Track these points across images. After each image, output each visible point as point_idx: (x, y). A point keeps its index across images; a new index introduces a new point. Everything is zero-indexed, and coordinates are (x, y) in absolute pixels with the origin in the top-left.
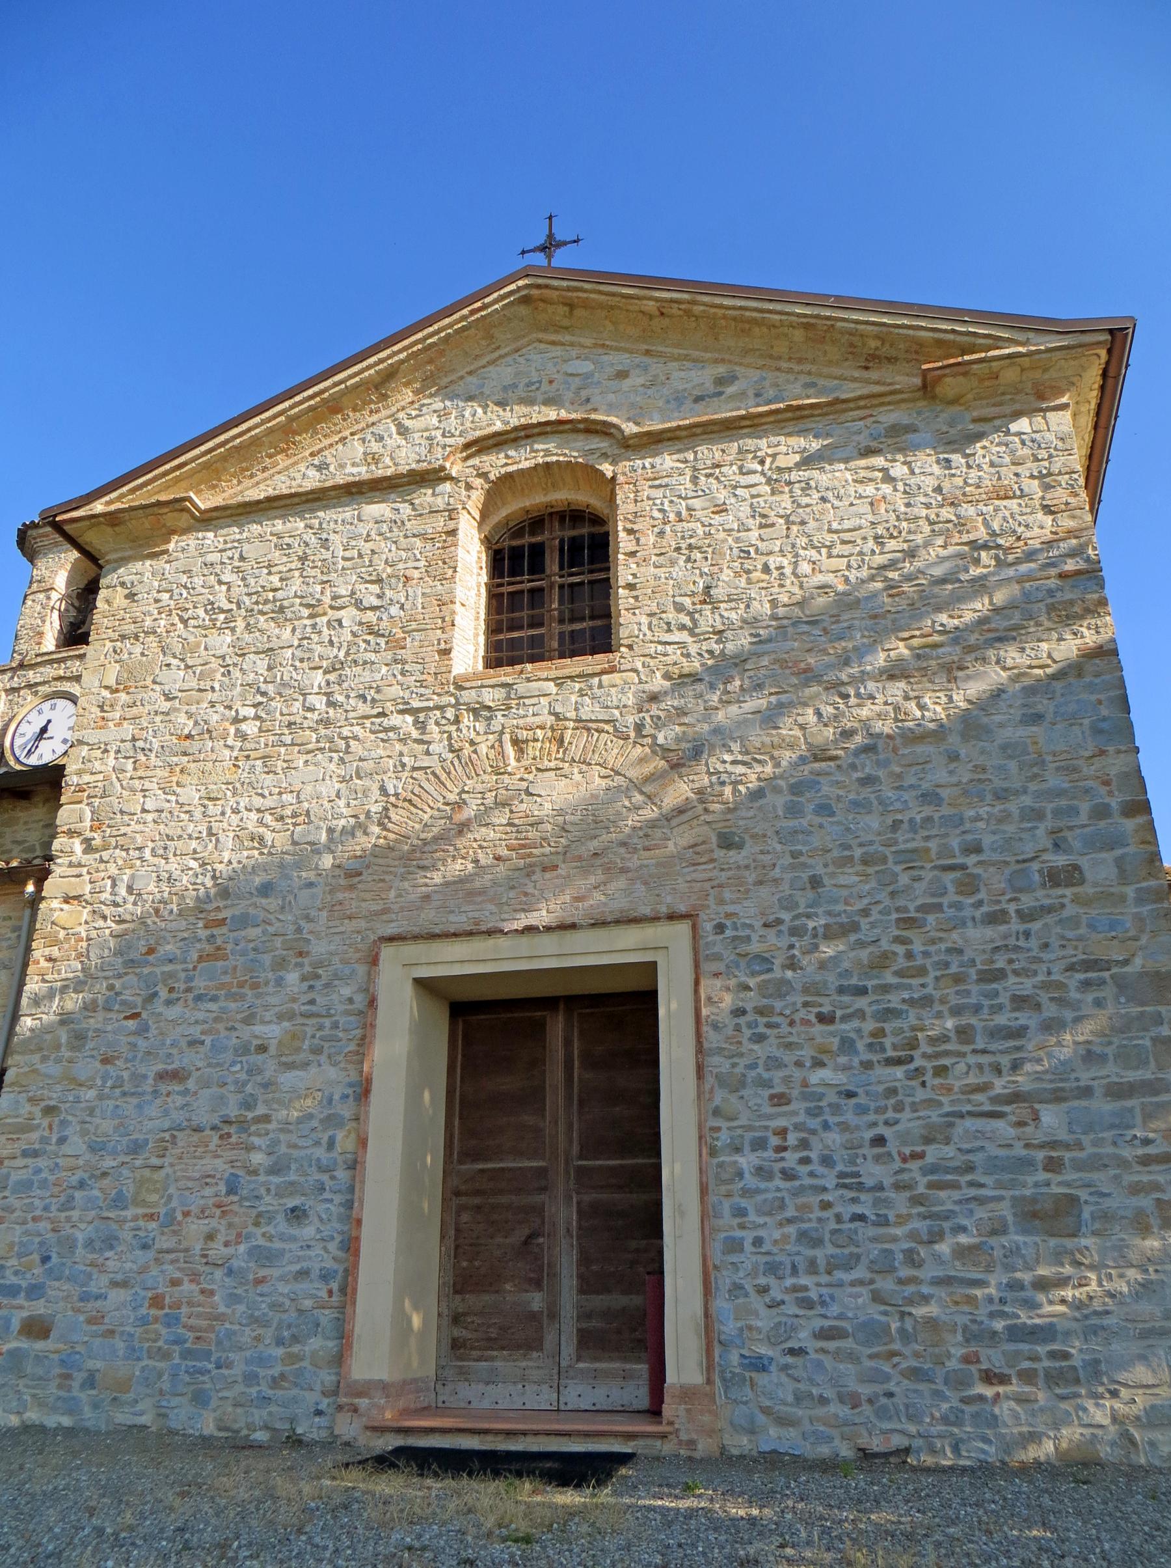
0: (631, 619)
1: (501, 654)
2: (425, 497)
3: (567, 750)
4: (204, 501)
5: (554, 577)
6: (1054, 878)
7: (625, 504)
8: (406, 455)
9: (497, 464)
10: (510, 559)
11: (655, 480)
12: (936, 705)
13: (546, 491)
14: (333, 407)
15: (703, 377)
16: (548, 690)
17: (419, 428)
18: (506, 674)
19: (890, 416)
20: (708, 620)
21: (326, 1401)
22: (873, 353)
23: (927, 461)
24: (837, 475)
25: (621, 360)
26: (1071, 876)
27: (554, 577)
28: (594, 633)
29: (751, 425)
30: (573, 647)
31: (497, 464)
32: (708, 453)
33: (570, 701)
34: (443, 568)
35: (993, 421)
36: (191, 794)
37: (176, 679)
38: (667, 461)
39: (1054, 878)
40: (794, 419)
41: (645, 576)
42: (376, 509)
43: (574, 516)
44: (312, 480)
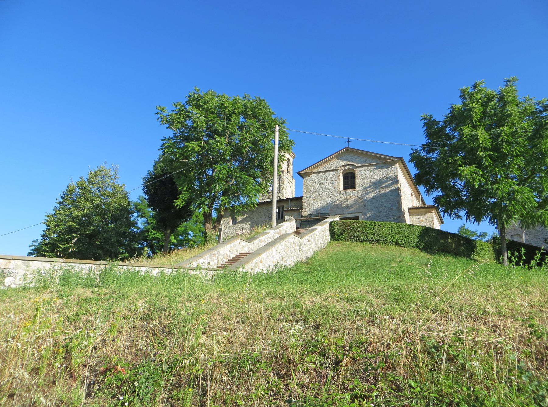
0: (357, 185)
1: (345, 188)
2: (336, 171)
3: (353, 195)
4: (313, 171)
5: (349, 181)
6: (391, 209)
7: (356, 173)
8: (334, 167)
9: (344, 168)
10: (345, 177)
11: (359, 171)
12: (387, 190)
13: (352, 162)
14: (327, 161)
15: (364, 160)
16: (349, 192)
17: (336, 163)
18: (345, 190)
19: (382, 165)
20: (364, 186)
21: (78, 190)
22: (380, 159)
23: (384, 170)
24: (376, 171)
25: (356, 157)
26: (392, 209)
27: (349, 181)
28: (353, 186)
29: (369, 166)
30: (351, 188)
31: (344, 168)
32: (364, 168)
33: (352, 193)
34: (339, 179)
35: (391, 166)
36: (316, 202)
37: (313, 190)
38: (360, 169)
39: (391, 209)
40: (372, 165)
41: (358, 181)
42: (332, 173)
43: (351, 173)
44: (325, 170)
